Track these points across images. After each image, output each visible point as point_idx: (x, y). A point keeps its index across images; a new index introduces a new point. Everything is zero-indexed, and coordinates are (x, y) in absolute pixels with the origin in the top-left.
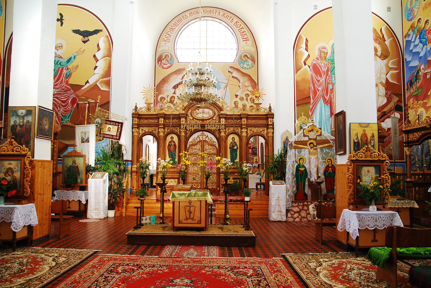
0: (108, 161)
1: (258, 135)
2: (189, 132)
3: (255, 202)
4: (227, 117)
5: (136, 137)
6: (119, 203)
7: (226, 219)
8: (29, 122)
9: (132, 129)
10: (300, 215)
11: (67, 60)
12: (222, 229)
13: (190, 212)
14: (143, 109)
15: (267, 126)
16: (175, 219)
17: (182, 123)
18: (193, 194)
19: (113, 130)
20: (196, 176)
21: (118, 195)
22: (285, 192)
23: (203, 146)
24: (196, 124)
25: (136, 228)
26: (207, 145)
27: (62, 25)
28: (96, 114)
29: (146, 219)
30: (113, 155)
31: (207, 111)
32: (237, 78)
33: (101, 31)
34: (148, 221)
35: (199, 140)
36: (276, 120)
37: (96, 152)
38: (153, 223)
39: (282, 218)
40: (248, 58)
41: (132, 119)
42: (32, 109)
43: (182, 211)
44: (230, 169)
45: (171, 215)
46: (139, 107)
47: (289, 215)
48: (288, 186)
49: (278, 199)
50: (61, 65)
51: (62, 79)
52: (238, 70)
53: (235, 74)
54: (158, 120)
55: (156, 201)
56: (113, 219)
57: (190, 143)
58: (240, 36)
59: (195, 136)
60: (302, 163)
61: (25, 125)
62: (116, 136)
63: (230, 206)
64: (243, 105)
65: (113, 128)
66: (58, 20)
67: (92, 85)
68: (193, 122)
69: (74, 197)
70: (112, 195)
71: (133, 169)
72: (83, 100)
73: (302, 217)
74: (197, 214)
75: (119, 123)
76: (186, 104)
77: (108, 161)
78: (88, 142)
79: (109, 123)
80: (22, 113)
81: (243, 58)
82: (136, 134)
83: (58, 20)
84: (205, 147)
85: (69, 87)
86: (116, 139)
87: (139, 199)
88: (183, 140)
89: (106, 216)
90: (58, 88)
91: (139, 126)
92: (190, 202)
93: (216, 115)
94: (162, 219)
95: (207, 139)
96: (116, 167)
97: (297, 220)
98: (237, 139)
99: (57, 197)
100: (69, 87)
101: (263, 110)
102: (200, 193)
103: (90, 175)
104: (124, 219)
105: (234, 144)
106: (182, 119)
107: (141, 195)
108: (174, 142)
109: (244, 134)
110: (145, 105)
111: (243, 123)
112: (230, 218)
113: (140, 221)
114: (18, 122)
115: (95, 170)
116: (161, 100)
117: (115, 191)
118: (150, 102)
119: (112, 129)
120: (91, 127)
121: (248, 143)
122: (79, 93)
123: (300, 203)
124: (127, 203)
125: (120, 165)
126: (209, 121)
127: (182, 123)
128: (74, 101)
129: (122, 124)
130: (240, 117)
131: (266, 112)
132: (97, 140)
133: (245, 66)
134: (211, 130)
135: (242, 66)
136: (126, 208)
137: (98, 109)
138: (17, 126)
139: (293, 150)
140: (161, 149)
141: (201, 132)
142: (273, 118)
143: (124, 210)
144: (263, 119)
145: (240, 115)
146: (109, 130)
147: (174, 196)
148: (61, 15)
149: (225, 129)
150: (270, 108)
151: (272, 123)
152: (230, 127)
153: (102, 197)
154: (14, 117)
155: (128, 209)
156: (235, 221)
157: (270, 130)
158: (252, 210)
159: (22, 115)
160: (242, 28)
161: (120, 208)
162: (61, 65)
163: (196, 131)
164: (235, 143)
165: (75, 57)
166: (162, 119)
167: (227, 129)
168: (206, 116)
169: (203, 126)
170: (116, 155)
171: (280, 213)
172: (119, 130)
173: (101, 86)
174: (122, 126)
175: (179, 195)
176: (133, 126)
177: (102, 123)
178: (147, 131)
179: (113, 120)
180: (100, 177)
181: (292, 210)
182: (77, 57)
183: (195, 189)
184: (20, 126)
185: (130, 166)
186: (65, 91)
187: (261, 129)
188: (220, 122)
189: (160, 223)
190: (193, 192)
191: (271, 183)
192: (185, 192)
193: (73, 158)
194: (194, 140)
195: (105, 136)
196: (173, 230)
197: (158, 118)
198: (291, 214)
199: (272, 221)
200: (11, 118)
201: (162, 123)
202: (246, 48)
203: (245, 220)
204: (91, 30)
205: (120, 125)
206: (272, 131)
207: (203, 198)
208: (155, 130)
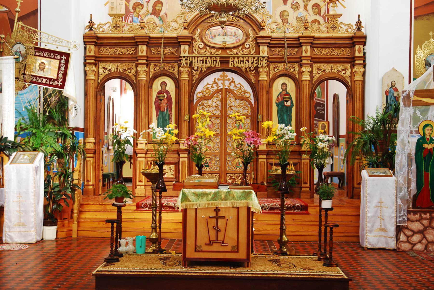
0: (41, 129)
1: (327, 79)
2: (197, 73)
3: (336, 211)
4: (273, 43)
5: (92, 82)
6: (63, 212)
7: (282, 243)
9: (85, 66)
10: (425, 237)
12: (276, 261)
13: (217, 230)
14: (106, 27)
15: (352, 61)
16: (188, 242)
17: (183, 54)
18: (223, 196)
19: (51, 68)
20: (211, 160)
21: (64, 197)
22: (394, 192)
23: (223, 101)
24: (211, 57)
25: (109, 261)
26: (233, 99)
28: (13, 35)
29: (127, 244)
30: (50, 119)
31: (233, 31)
34: (130, 247)
35: (215, 88)
36: (371, 49)
37: (18, 112)
38: (140, 251)
39: (387, 243)
41: (82, 45)
43: (201, 227)
44: (292, 145)
45: (180, 237)
46: (96, 22)
47: (402, 237)
48: (401, 180)
49: (380, 205)
54: (136, 49)
55: (135, 208)
56: (54, 244)
57: (199, 95)
59: (209, 80)
60: (430, 134)
62: (57, 80)
63: (287, 218)
64: (297, 18)
65: (49, 65)
68: (205, 53)
70: (50, 197)
71: (88, 146)
73: (429, 242)
74: (231, 233)
75: (61, 54)
76: (190, 17)
77: (41, 129)
79: (41, 53)
82: (91, 76)
84: (228, 102)
86: (57, 86)
87: (114, 205)
88: (185, 88)
89: (39, 239)
91: (98, 60)
92: (217, 210)
94: (157, 244)
95: (232, 87)
96: (58, 141)
97: (419, 247)
98: (291, 87)
101: (344, 28)
102: (238, 192)
103: (6, 158)
104: (74, 245)
105: (284, 96)
106: (183, 47)
107: (119, 195)
108: (167, 92)
109: (306, 77)
110: (110, 19)
111: (304, 54)
112: (287, 242)
113: (116, 248)
115: (15, 147)
116: (134, 9)
117: (57, 189)
118: (118, 13)
119: (47, 67)
120: (4, 61)
121: (312, 94)
123: (425, 213)
124: (80, 212)
125: (65, 136)
126: (236, 50)
127: (183, 54)
129: (68, 55)
130: (297, 43)
131: (350, 33)
132: (18, 89)
134: (240, 69)
136: (79, 222)
137: (18, 25)
139: (411, 109)
140: (143, 106)
141: (220, 73)
142: (365, 44)
143: (74, 226)
144: (345, 47)
145: (298, 39)
146: (42, 67)
147: (185, 198)
149: (268, 66)
150: (359, 23)
151: (362, 55)
152: (277, 62)
153: (32, 200)
155: (82, 224)
156: (301, 247)
157: (358, 69)
158: (337, 226)
161: (66, 222)
163: (211, 71)
164: (288, 94)
166: (144, 47)
167: (272, 66)
168: (230, 41)
169: (224, 61)
170: (57, 117)
171: (383, 233)
172: (62, 69)
174: (67, 61)
175: (196, 197)
176: (85, 60)
177: (27, 54)
178: (113, 70)
179: (49, 47)
180: (28, 161)
181: (407, 228)
183: (226, 184)
185: (81, 140)
187: (340, 67)
188: (257, 52)
189: (154, 252)
190: (223, 190)
191: (364, 173)
192: (208, 191)
194: (207, 89)
195: (35, 80)
196: (184, 265)
197: (136, 45)
198: (405, 234)
199: (368, 249)
201: (144, 54)
203: (320, 247)
205: (64, 57)
206: (362, 70)
207: (242, 203)
208: (130, 69)
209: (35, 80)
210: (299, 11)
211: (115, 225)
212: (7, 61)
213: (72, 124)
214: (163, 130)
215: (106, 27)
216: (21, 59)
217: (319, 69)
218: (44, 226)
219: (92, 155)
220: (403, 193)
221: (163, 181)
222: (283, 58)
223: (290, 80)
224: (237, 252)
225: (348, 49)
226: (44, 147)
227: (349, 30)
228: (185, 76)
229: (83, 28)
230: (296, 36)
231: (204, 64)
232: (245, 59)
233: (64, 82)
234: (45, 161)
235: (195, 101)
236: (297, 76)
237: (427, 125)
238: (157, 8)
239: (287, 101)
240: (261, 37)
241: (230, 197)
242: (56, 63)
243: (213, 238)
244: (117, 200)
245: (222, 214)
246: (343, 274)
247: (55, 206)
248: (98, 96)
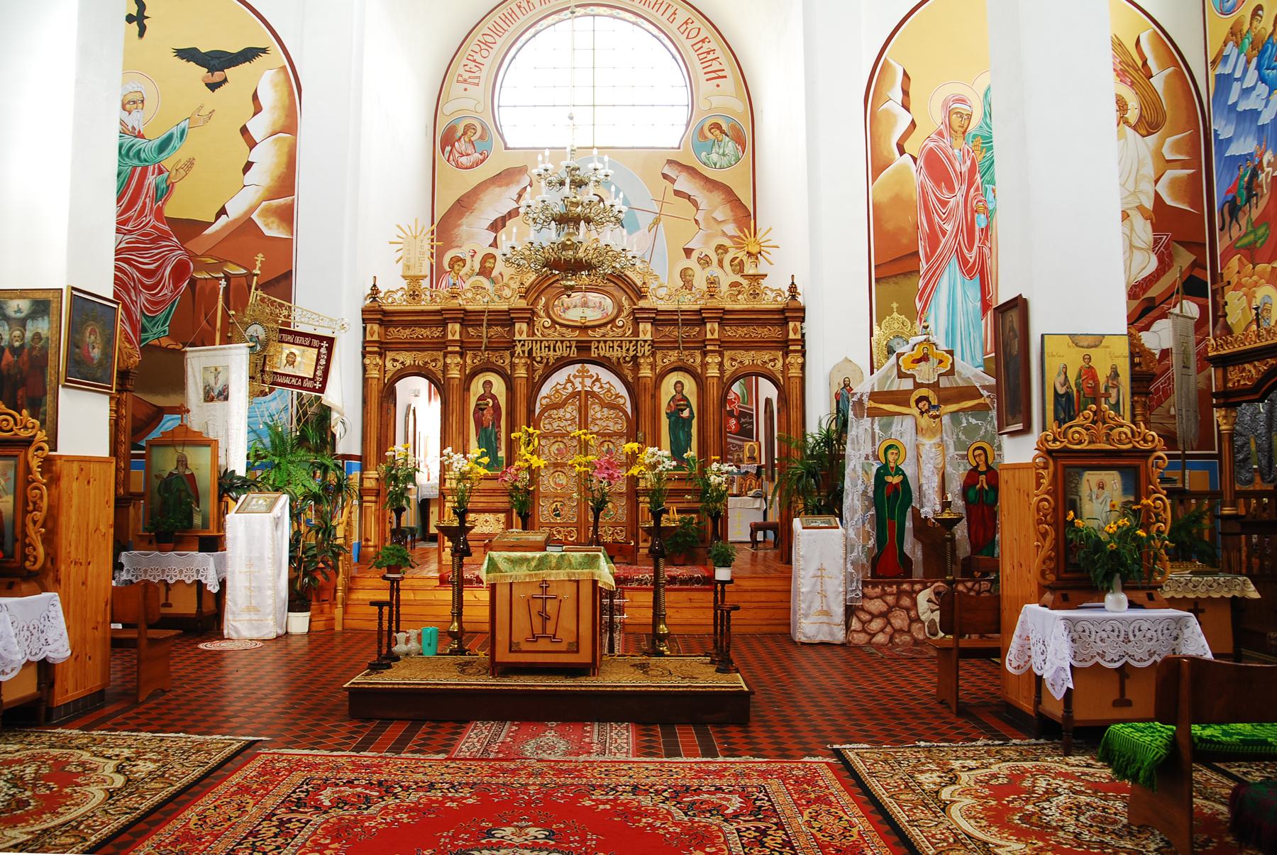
0: (289, 457)
2: (541, 366)
4: (659, 319)
6: (321, 589)
7: (657, 638)
8: (40, 339)
9: (364, 357)
10: (889, 623)
11: (157, 142)
12: (643, 667)
13: (545, 618)
14: (397, 296)
15: (784, 346)
17: (517, 337)
18: (553, 565)
19: (304, 362)
20: (564, 505)
21: (321, 565)
22: (842, 552)
24: (562, 342)
25: (375, 668)
26: (597, 408)
27: (141, 34)
29: (408, 640)
30: (302, 440)
31: (597, 300)
32: (689, 198)
33: (264, 51)
34: (413, 645)
35: (570, 390)
36: (813, 327)
37: (252, 430)
38: (429, 652)
39: (831, 634)
40: (722, 132)
41: (361, 325)
42: (50, 296)
44: (669, 479)
47: (855, 624)
49: (820, 574)
51: (145, 203)
53: (684, 183)
56: (306, 639)
57: (544, 402)
59: (560, 377)
60: (895, 461)
61: (27, 347)
62: (313, 379)
63: (669, 598)
65: (302, 357)
66: (130, 19)
69: (181, 572)
70: (299, 565)
71: (368, 484)
73: (895, 631)
74: (567, 622)
75: (321, 338)
76: (531, 278)
77: (289, 457)
78: (226, 398)
79: (290, 338)
80: (19, 311)
81: (709, 135)
82: (374, 373)
83: (130, 19)
84: (591, 412)
85: (166, 228)
86: (313, 389)
87: (384, 578)
88: (521, 390)
89: (281, 632)
90: (130, 232)
91: (384, 348)
92: (544, 585)
93: (625, 313)
94: (457, 640)
95: (596, 389)
96: (314, 477)
97: (880, 638)
98: (690, 387)
99: (128, 571)
100: (166, 228)
101: (771, 295)
102: (576, 556)
104: (338, 640)
106: (517, 326)
107: (393, 562)
108: (494, 397)
109: (713, 372)
110: (404, 284)
111: (709, 336)
112: (669, 634)
113: (389, 647)
115: (246, 485)
116: (451, 266)
117: (311, 553)
119: (298, 359)
122: (197, 246)
123: (890, 585)
124: (349, 590)
125: (325, 469)
126: (603, 330)
127: (517, 337)
128: (180, 271)
129: (331, 341)
130: (698, 318)
131: (781, 302)
132: (253, 394)
133: (714, 157)
135: (704, 159)
136: (345, 606)
137: (255, 295)
139: (866, 422)
140: (454, 420)
141: (578, 366)
142: (803, 320)
143: (338, 612)
144: (773, 325)
145: (699, 312)
146: (291, 361)
147: (493, 566)
149: (653, 354)
150: (793, 288)
151: (799, 337)
152: (668, 348)
153: (269, 570)
155: (351, 610)
156: (687, 644)
157: (794, 359)
158: (737, 608)
159: (19, 315)
160: (703, 41)
163: (562, 363)
166: (457, 326)
167: (659, 355)
168: (593, 316)
169: (583, 347)
170: (314, 440)
171: (825, 619)
172: (323, 362)
173: (267, 225)
174: (330, 350)
175: (508, 563)
176: (364, 348)
178: (408, 363)
180: (264, 509)
181: (862, 609)
182: (190, 134)
183: (559, 543)
185: (356, 475)
186: (153, 241)
187: (766, 356)
188: (636, 333)
189: (452, 652)
190: (554, 552)
191: (797, 523)
192: (529, 555)
193: (180, 449)
194: (557, 391)
195: (278, 381)
196: (493, 674)
197: (444, 323)
198: (859, 619)
201: (457, 337)
202: (717, 102)
204: (234, 48)
205: (325, 344)
206: (800, 360)
207: (583, 574)
208: (434, 360)
209: (280, 380)
210: (708, 269)
211: (386, 610)
213: (340, 450)
214: (465, 457)
215: (397, 296)
216: (258, 348)
217: (733, 360)
218: (289, 611)
219: (373, 498)
220: (855, 554)
221: (465, 539)
222: (676, 342)
223: (687, 376)
224: (577, 652)
225: (778, 328)
226: (292, 486)
227: (779, 299)
228: (521, 372)
229: (362, 299)
230: (697, 307)
231: (552, 353)
232: (616, 344)
233: (324, 382)
234: (291, 508)
235: (537, 411)
237: (890, 447)
238: (487, 265)
239: (682, 410)
241: (565, 564)
242: (313, 353)
243: (538, 631)
244: (391, 569)
245: (552, 592)
246: (743, 684)
247: (306, 580)
248: (385, 404)
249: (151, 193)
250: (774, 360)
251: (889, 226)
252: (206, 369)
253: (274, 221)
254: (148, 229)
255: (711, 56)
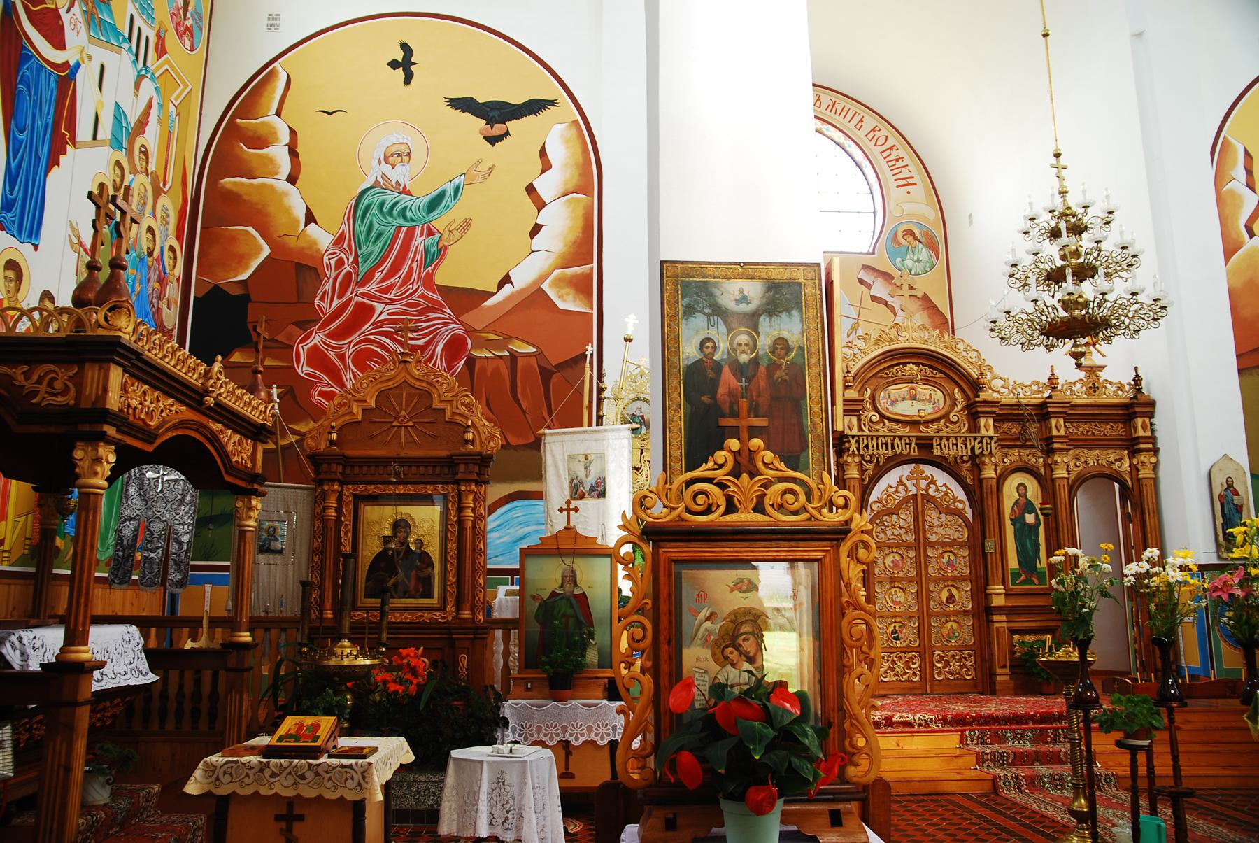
4: (1009, 414)
8: (788, 349)
11: (427, 199)
15: (1132, 445)
23: (918, 518)
26: (934, 514)
27: (408, 81)
32: (886, 303)
33: (552, 103)
35: (903, 494)
40: (916, 238)
42: (799, 276)
50: (405, 217)
51: (411, 269)
52: (888, 277)
53: (880, 289)
58: (889, 174)
61: (764, 363)
66: (394, 64)
67: (522, 291)
68: (883, 430)
69: (590, 729)
72: (488, 345)
78: (602, 495)
80: (744, 299)
81: (902, 241)
83: (394, 64)
85: (438, 297)
90: (393, 301)
93: (959, 407)
95: (931, 492)
99: (514, 730)
100: (438, 297)
101: (1111, 388)
111: (1055, 433)
114: (723, 346)
122: (475, 318)
126: (936, 426)
128: (455, 347)
130: (1042, 412)
131: (1125, 396)
133: (909, 263)
135: (899, 265)
138: (718, 367)
142: (1151, 415)
144: (1116, 421)
148: (405, 47)
150: (1137, 380)
151: (1148, 434)
154: (699, 320)
159: (743, 307)
160: (891, 148)
162: (405, 217)
165: (457, 190)
173: (560, 297)
182: (466, 192)
184: (739, 370)
186: (421, 313)
188: (974, 428)
193: (568, 561)
194: (889, 495)
200: (683, 324)
202: (909, 208)
204: (517, 99)
212: (555, 438)
217: (1077, 459)
232: (960, 441)
236: (1042, 471)
240: (985, 401)
249: (419, 257)
250: (1120, 460)
251: (1246, 313)
252: (571, 457)
253: (569, 292)
254: (415, 298)
255: (899, 164)
